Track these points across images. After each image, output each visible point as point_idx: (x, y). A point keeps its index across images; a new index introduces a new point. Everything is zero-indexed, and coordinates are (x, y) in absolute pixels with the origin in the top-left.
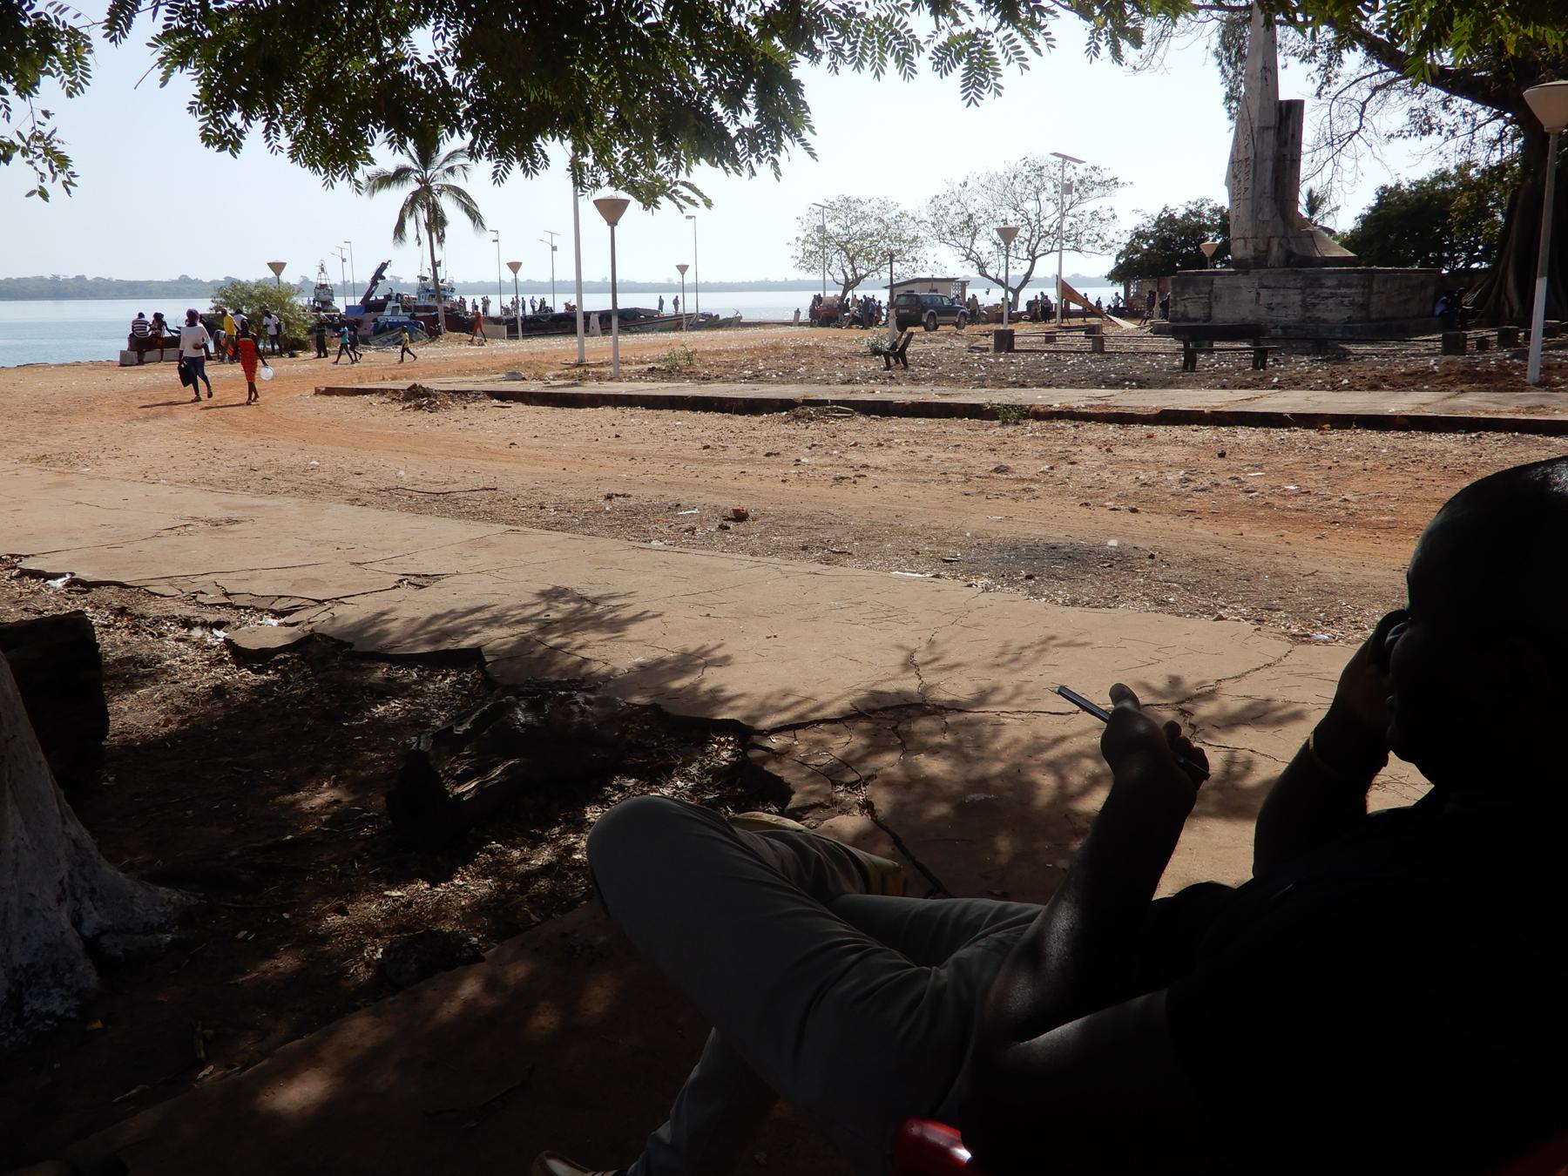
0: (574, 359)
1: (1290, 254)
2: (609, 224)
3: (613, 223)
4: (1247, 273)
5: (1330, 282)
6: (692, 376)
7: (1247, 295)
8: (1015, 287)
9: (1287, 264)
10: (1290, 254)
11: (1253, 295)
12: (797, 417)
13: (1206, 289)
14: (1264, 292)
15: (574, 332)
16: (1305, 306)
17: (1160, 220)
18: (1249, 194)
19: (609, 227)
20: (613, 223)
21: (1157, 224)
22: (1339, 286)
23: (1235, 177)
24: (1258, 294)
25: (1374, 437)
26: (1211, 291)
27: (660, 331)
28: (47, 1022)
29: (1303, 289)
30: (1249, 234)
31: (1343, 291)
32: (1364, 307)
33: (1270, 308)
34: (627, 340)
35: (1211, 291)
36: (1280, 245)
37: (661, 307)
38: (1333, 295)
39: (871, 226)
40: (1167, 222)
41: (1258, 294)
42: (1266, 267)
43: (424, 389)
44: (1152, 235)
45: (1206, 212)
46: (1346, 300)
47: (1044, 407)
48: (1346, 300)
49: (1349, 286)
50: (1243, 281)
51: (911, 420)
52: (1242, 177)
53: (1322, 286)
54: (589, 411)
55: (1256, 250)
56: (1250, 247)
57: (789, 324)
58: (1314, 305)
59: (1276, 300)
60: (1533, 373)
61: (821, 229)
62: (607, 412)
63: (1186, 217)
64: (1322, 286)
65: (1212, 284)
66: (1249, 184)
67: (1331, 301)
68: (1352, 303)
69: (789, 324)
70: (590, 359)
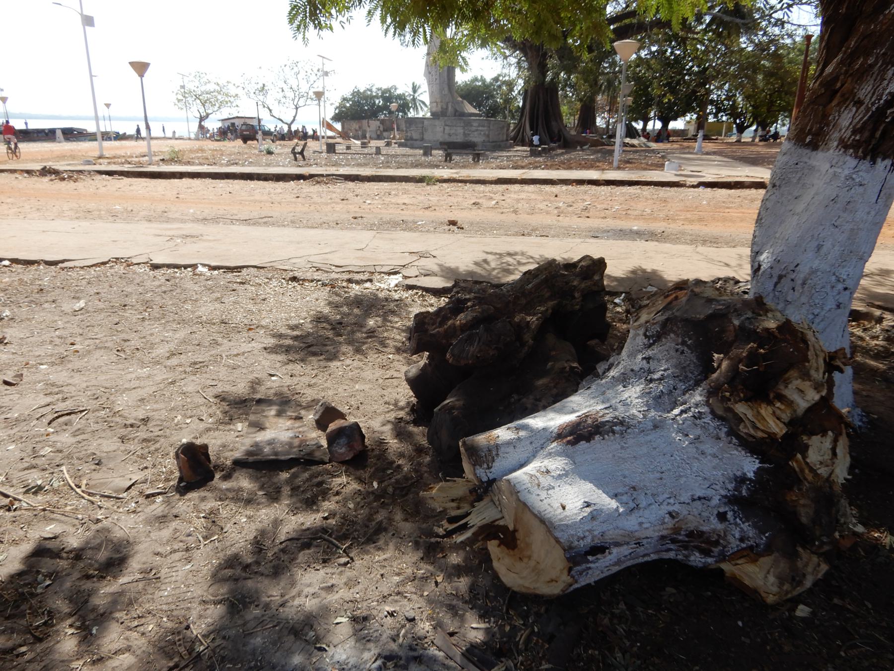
0: (97, 154)
1: (456, 111)
2: (139, 76)
3: (141, 75)
4: (439, 119)
5: (475, 124)
6: (180, 162)
7: (439, 129)
8: (289, 122)
9: (455, 115)
10: (456, 111)
11: (442, 129)
12: (318, 182)
13: (421, 125)
14: (447, 128)
15: (96, 140)
16: (465, 134)
17: (354, 92)
18: (438, 81)
19: (139, 78)
20: (141, 75)
21: (353, 94)
22: (479, 126)
23: (430, 73)
24: (444, 129)
25: (724, 191)
26: (423, 127)
27: (90, 140)
28: (748, 641)
29: (464, 127)
30: (439, 100)
31: (480, 128)
32: (488, 136)
33: (450, 135)
34: (106, 144)
35: (423, 127)
36: (452, 106)
37: (368, 123)
38: (477, 130)
39: (211, 87)
40: (357, 93)
41: (444, 129)
42: (446, 116)
43: (54, 169)
44: (350, 99)
45: (374, 89)
46: (482, 133)
47: (467, 177)
48: (482, 133)
49: (483, 126)
50: (437, 122)
51: (377, 183)
52: (433, 73)
53: (472, 126)
54: (176, 181)
55: (442, 108)
56: (439, 106)
57: (170, 138)
58: (469, 134)
59: (453, 131)
60: (615, 164)
61: (183, 87)
62: (186, 181)
63: (365, 91)
64: (472, 126)
65: (423, 123)
66: (437, 77)
67: (476, 133)
68: (485, 134)
69: (170, 138)
70: (106, 154)
